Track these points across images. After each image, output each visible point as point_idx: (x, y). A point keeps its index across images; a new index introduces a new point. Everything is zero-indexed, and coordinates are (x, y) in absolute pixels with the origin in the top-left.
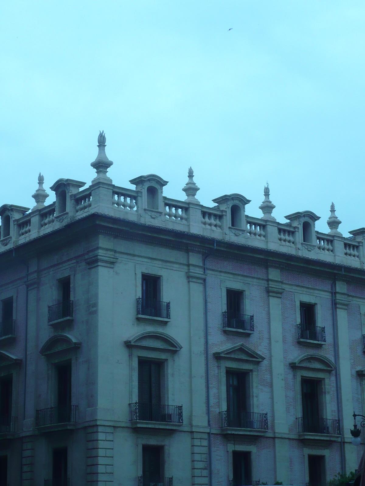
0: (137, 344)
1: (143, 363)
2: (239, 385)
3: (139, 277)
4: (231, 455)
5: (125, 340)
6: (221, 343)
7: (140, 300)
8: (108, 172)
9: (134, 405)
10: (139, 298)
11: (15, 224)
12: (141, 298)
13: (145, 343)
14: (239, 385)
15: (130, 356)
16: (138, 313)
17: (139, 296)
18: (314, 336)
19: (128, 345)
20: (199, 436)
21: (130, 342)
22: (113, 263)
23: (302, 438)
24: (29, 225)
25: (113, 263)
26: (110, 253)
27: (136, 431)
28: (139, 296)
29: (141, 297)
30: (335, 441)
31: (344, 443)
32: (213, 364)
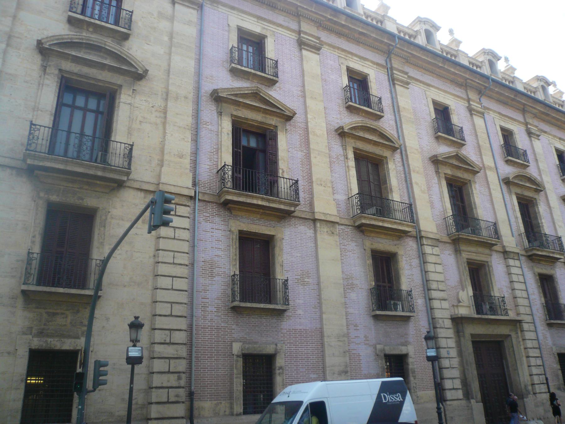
1: (360, 157)
2: (459, 191)
4: (236, 236)
6: (508, 171)
14: (459, 191)
15: (44, 68)
18: (367, 101)
20: (430, 242)
21: (342, 128)
23: (530, 253)
30: (405, 233)
31: (421, 237)
32: (209, 111)
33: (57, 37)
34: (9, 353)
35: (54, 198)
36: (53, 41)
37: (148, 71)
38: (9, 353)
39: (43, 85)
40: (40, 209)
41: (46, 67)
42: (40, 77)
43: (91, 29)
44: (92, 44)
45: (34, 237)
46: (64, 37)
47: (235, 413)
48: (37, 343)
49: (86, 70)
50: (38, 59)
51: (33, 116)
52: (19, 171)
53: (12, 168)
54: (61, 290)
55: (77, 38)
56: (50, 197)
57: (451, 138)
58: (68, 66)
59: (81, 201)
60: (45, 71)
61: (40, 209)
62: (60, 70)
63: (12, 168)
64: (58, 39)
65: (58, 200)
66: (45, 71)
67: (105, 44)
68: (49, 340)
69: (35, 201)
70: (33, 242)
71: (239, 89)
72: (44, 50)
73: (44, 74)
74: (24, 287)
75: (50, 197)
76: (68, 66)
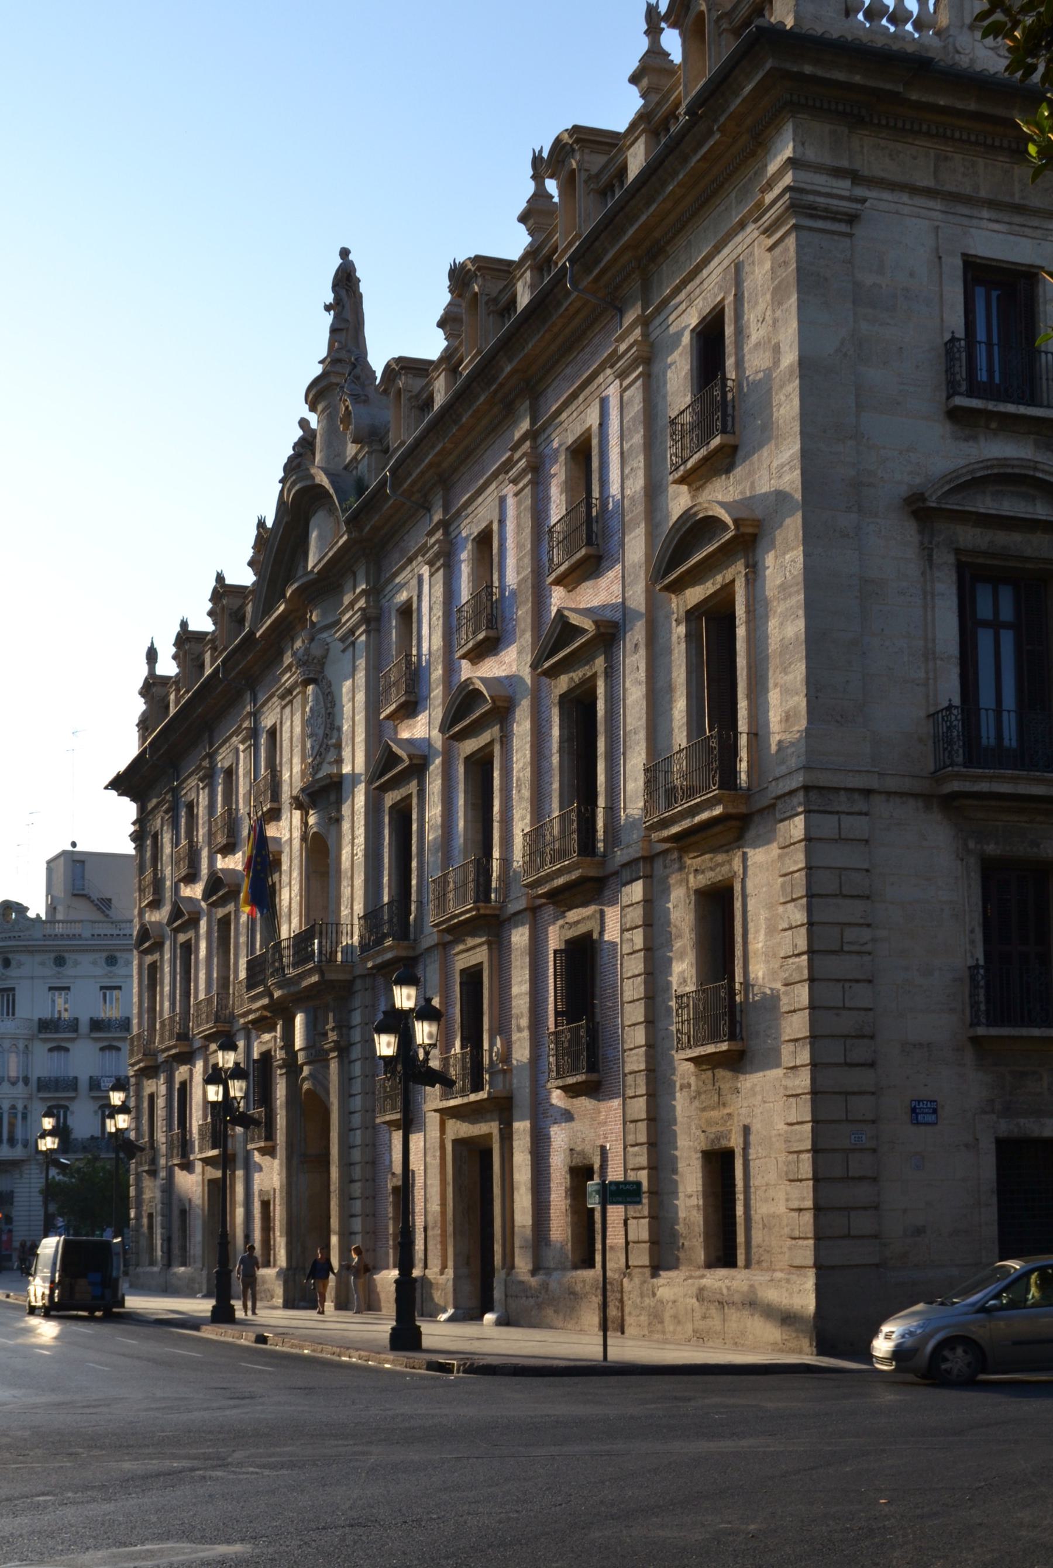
0: (952, 504)
3: (954, 265)
5: (904, 491)
7: (955, 712)
8: (320, 362)
9: (943, 717)
10: (949, 708)
11: (722, 33)
12: (956, 707)
13: (986, 504)
15: (927, 554)
16: (952, 390)
17: (950, 700)
19: (921, 510)
22: (852, 219)
24: (609, 193)
25: (852, 219)
26: (843, 186)
27: (951, 805)
28: (950, 700)
29: (957, 701)
33: (949, 477)
34: (967, 1146)
35: (991, 849)
36: (942, 487)
37: (645, 33)
38: (967, 1146)
39: (933, 595)
40: (972, 874)
41: (932, 549)
42: (923, 574)
43: (993, 425)
44: (1010, 474)
45: (972, 931)
46: (960, 472)
47: (641, 864)
48: (1005, 1128)
49: (1003, 539)
50: (910, 530)
51: (927, 673)
52: (927, 799)
53: (915, 796)
54: (1036, 1032)
55: (983, 468)
56: (985, 847)
57: (1023, 410)
58: (970, 537)
59: (1035, 850)
60: (930, 559)
61: (972, 874)
62: (958, 551)
63: (915, 796)
64: (951, 481)
65: (999, 852)
66: (930, 559)
67: (1035, 469)
68: (1022, 1121)
69: (962, 860)
70: (972, 942)
71: (1003, 462)
72: (921, 510)
73: (931, 568)
74: (971, 1033)
75: (985, 847)
76: (970, 537)
